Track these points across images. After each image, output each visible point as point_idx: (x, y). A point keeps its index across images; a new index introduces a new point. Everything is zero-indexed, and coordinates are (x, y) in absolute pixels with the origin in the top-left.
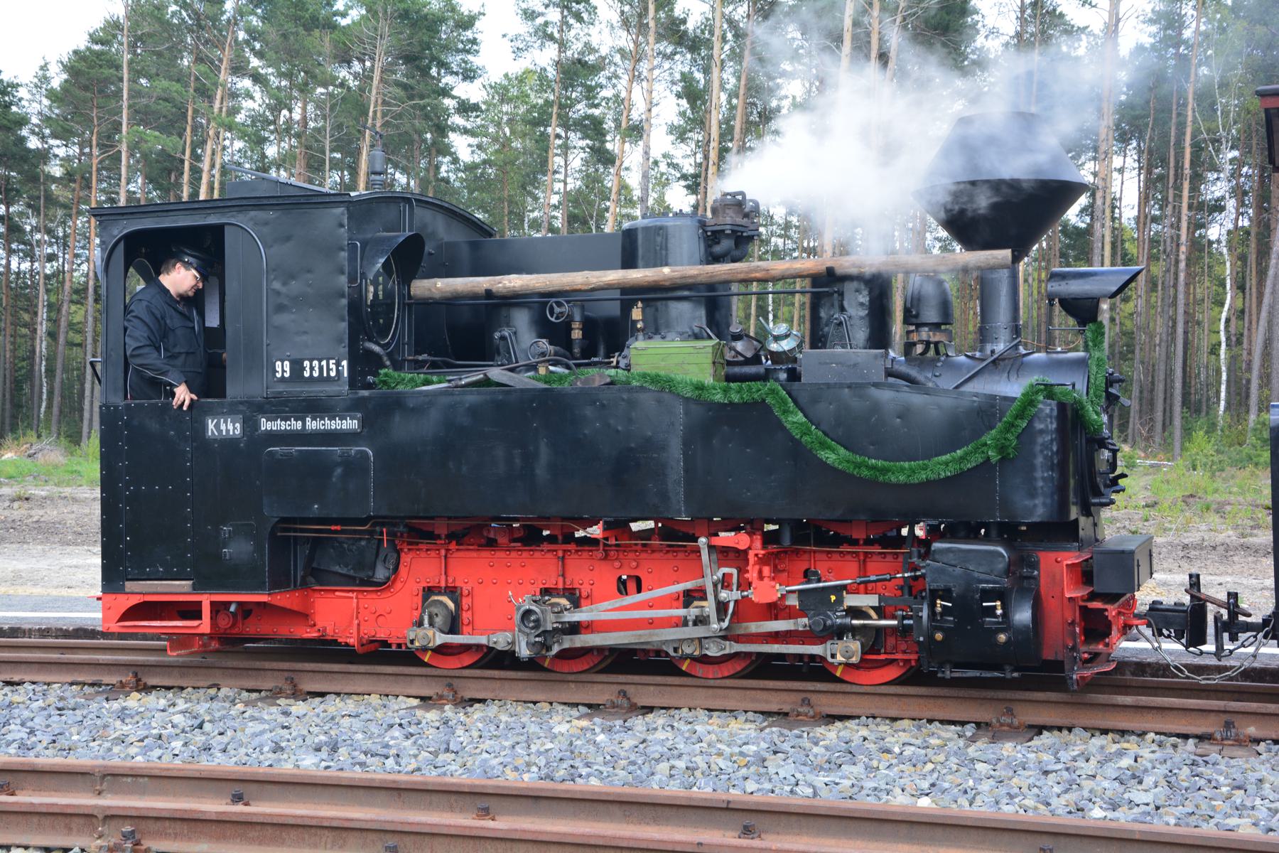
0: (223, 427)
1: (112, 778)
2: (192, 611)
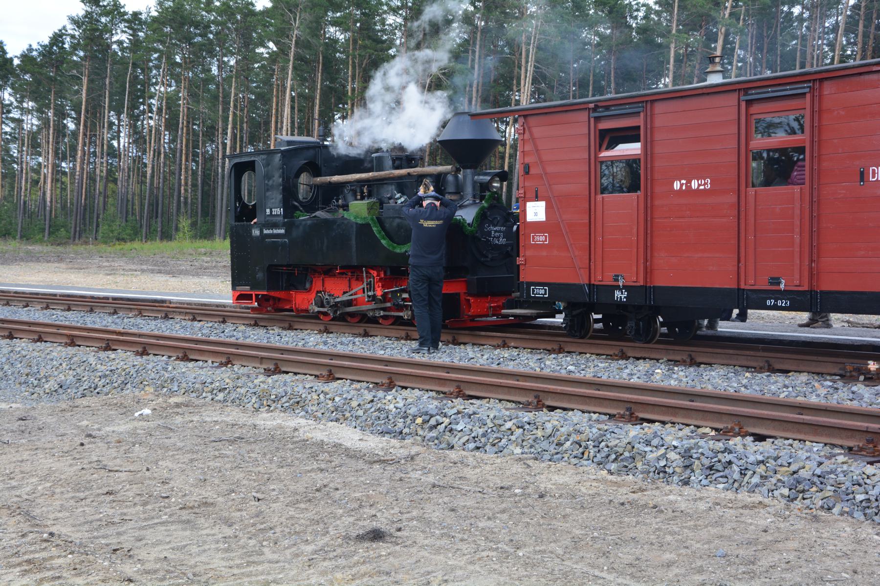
1: (140, 335)
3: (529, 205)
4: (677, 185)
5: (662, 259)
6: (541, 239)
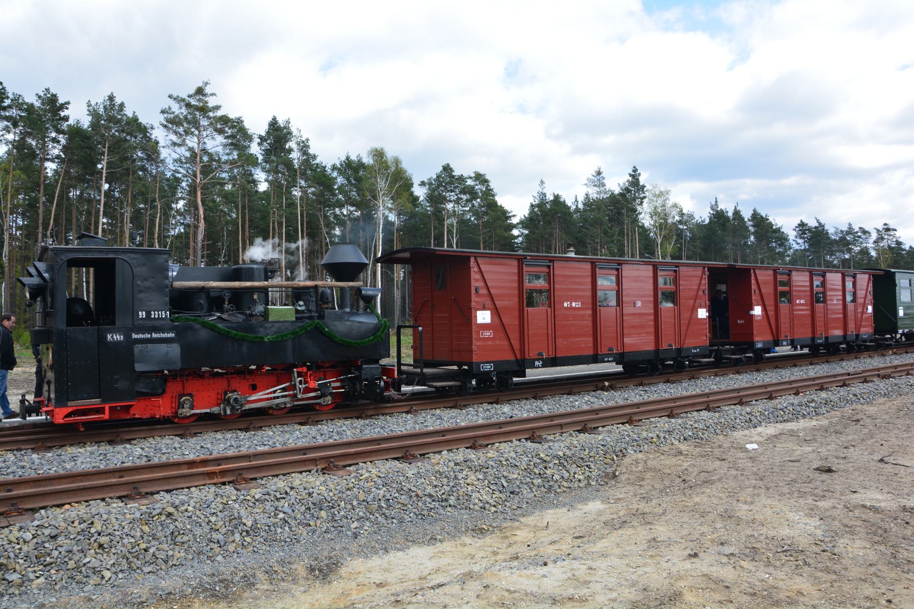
0: (115, 337)
2: (100, 411)
3: (699, 310)
4: (565, 305)
5: (560, 342)
6: (487, 334)
